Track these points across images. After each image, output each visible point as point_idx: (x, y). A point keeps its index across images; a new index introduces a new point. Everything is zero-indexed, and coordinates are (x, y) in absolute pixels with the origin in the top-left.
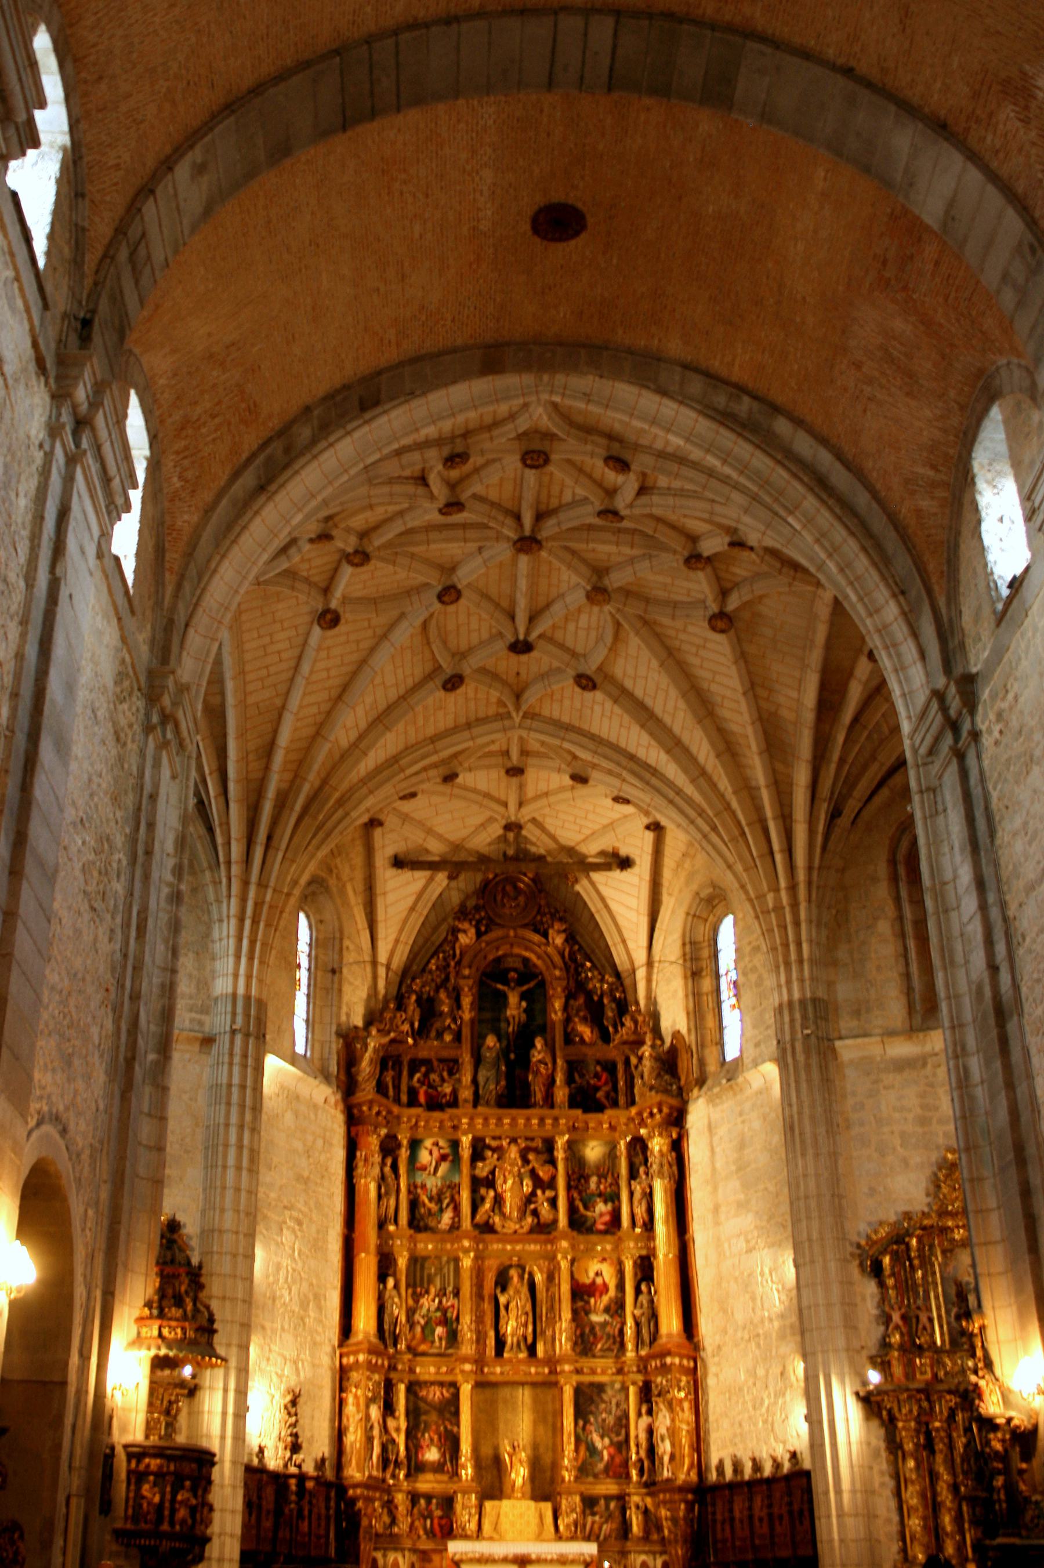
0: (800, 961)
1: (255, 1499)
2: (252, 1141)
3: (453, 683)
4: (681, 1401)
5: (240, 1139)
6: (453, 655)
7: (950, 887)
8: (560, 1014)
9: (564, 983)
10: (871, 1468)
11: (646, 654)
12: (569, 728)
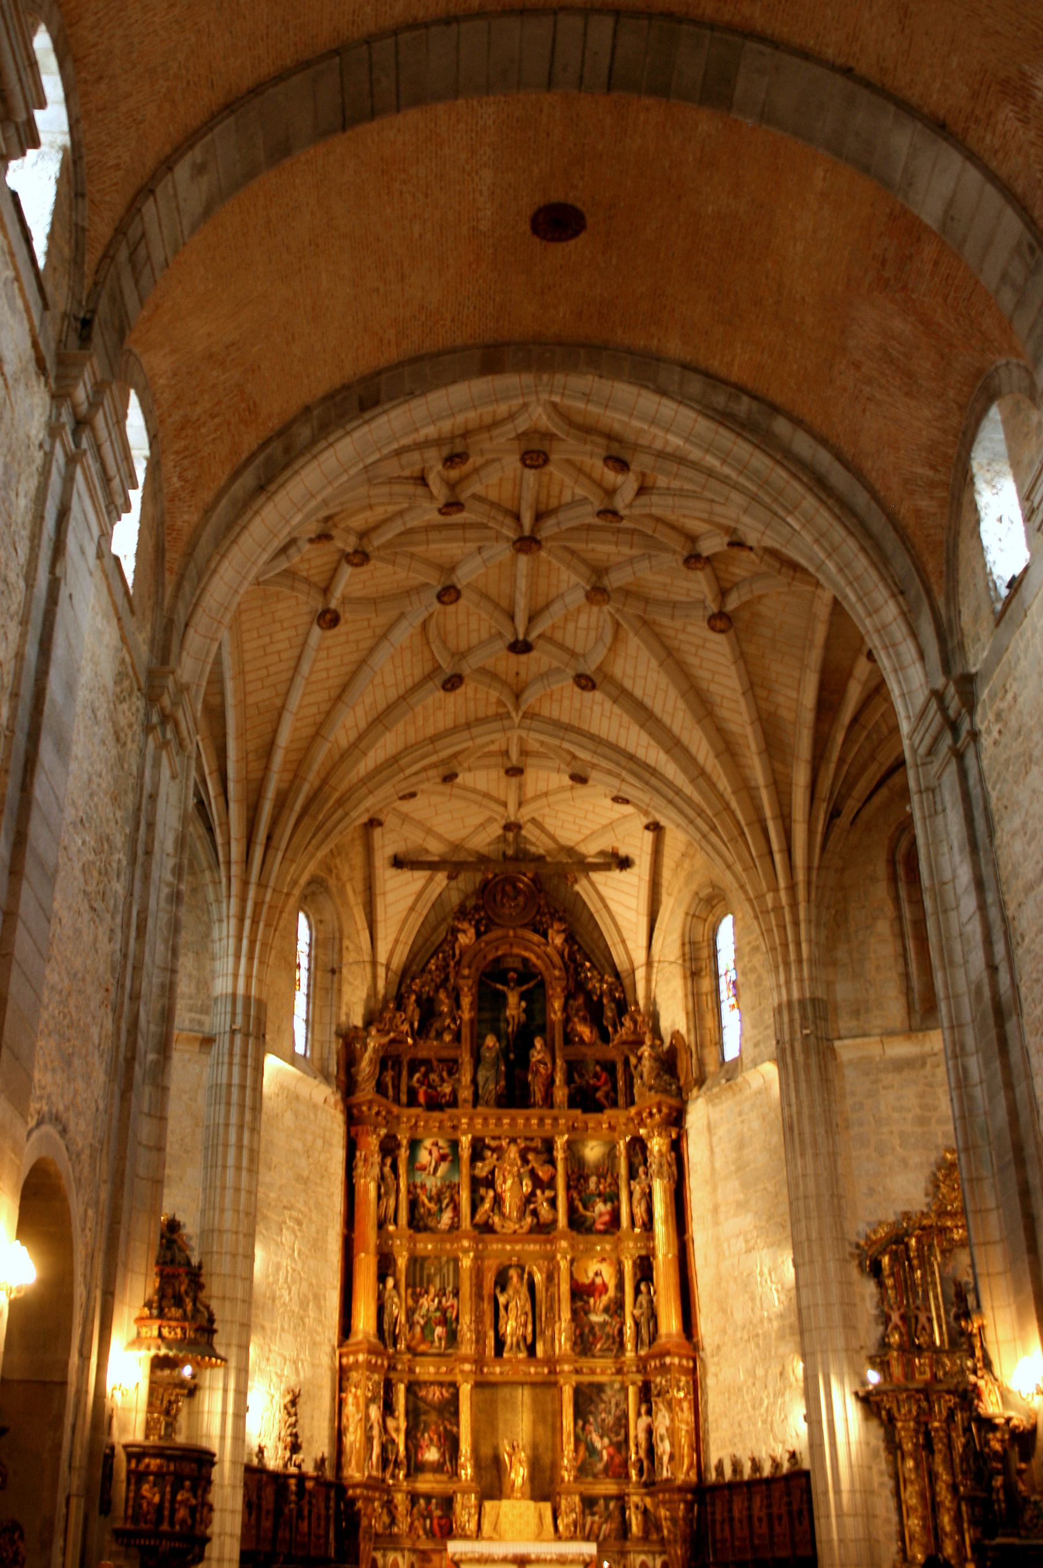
0: (800, 961)
1: (254, 1499)
2: (251, 1141)
3: (453, 683)
4: (680, 1401)
5: (240, 1139)
6: (453, 655)
7: (949, 887)
8: (559, 1014)
9: (564, 983)
10: (870, 1468)
11: (645, 654)
12: (568, 728)
